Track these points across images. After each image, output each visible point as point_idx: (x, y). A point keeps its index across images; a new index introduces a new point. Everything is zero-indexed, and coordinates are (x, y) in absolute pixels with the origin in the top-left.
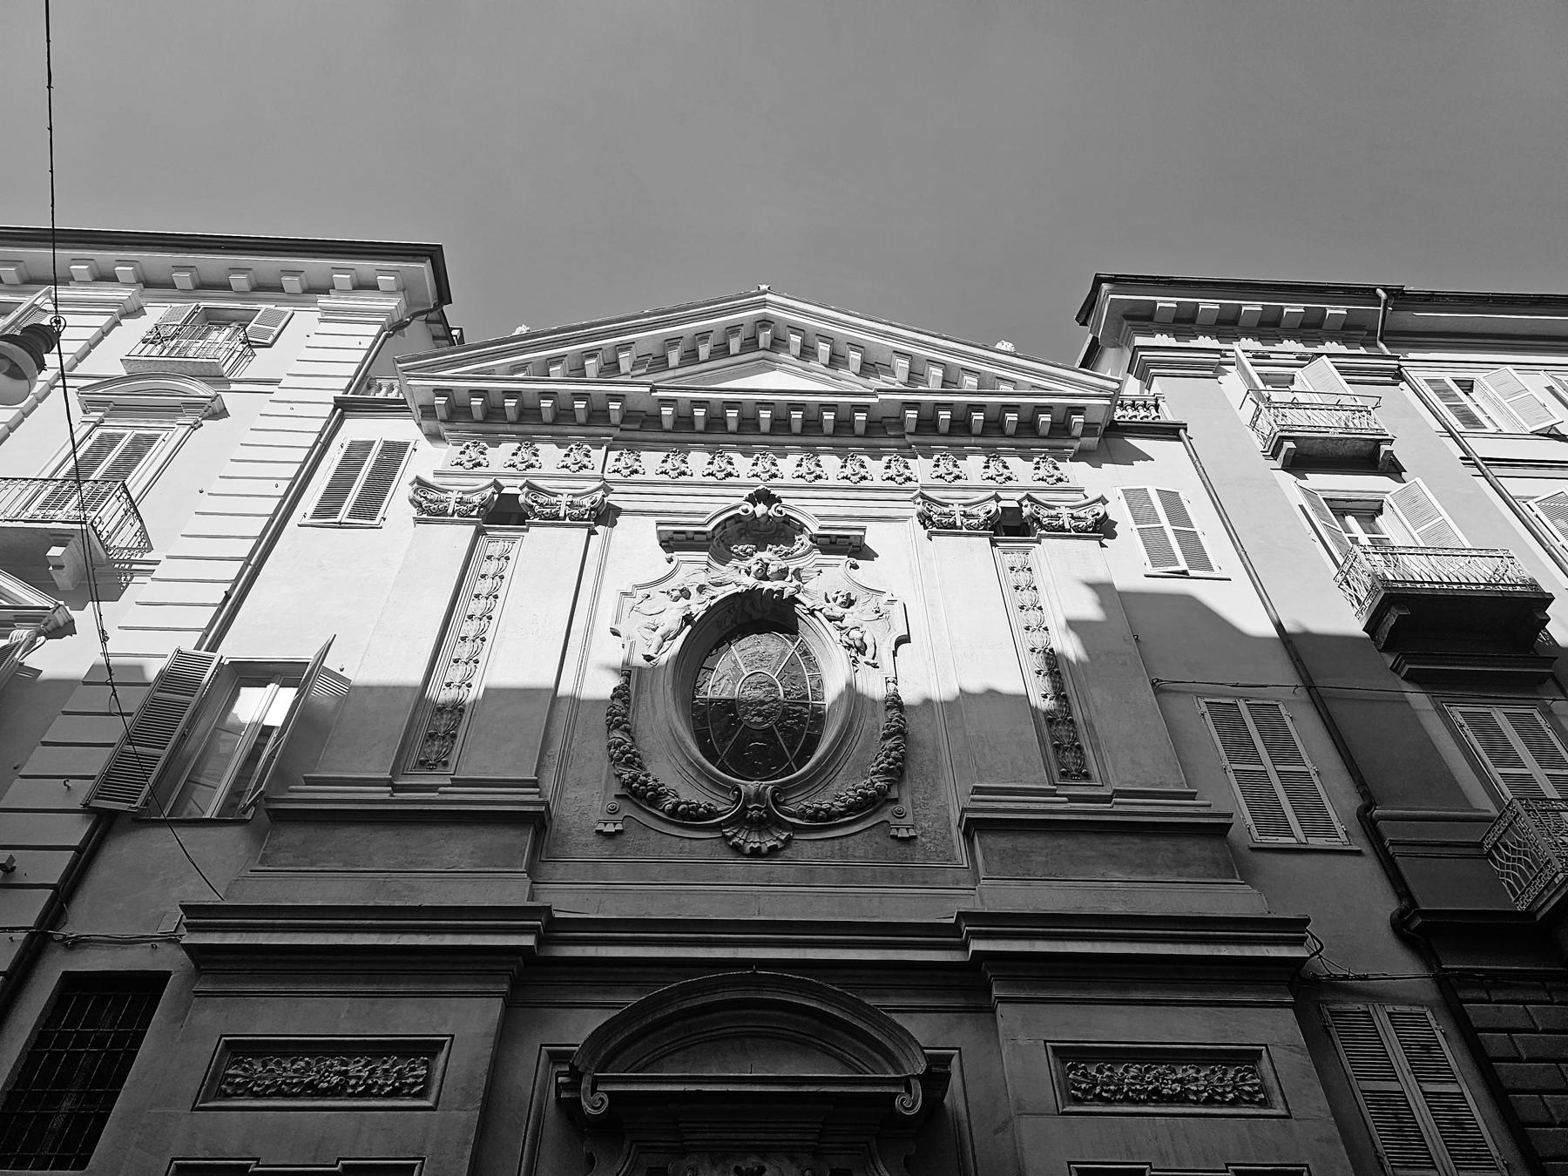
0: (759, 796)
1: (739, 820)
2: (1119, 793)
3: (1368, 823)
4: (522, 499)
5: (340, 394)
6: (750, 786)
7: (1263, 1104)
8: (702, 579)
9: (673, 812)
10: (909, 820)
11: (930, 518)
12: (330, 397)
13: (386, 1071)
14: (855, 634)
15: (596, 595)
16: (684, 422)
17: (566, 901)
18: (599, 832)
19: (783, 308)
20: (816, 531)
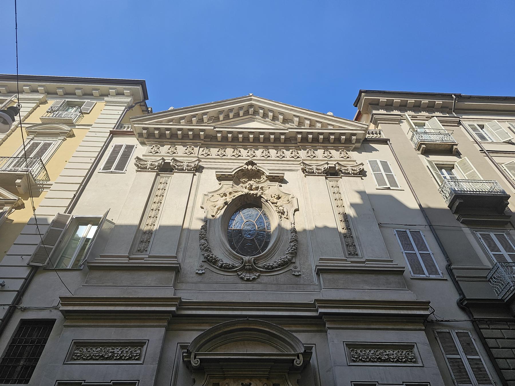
0: (249, 261)
1: (243, 269)
2: (368, 260)
3: (449, 270)
4: (171, 164)
5: (112, 129)
6: (246, 258)
7: (415, 362)
8: (231, 190)
9: (221, 267)
10: (298, 269)
11: (305, 170)
12: (108, 130)
13: (127, 351)
14: (281, 208)
15: (196, 195)
16: (225, 138)
17: (186, 296)
18: (197, 273)
19: (257, 101)
20: (268, 174)
